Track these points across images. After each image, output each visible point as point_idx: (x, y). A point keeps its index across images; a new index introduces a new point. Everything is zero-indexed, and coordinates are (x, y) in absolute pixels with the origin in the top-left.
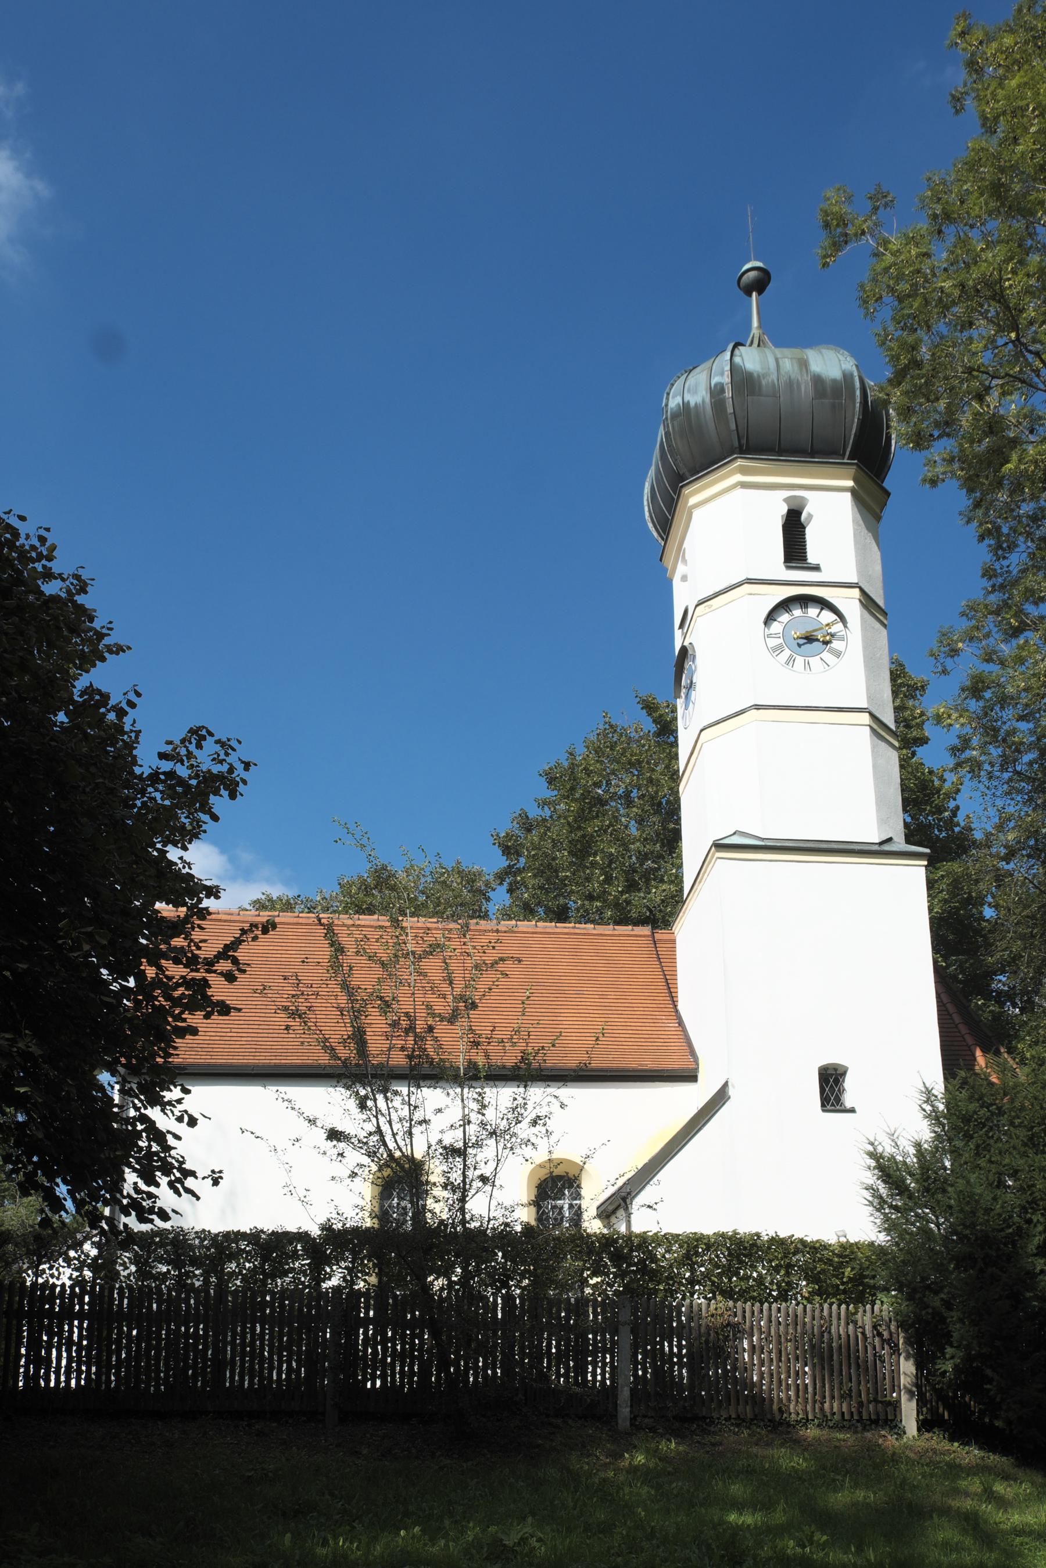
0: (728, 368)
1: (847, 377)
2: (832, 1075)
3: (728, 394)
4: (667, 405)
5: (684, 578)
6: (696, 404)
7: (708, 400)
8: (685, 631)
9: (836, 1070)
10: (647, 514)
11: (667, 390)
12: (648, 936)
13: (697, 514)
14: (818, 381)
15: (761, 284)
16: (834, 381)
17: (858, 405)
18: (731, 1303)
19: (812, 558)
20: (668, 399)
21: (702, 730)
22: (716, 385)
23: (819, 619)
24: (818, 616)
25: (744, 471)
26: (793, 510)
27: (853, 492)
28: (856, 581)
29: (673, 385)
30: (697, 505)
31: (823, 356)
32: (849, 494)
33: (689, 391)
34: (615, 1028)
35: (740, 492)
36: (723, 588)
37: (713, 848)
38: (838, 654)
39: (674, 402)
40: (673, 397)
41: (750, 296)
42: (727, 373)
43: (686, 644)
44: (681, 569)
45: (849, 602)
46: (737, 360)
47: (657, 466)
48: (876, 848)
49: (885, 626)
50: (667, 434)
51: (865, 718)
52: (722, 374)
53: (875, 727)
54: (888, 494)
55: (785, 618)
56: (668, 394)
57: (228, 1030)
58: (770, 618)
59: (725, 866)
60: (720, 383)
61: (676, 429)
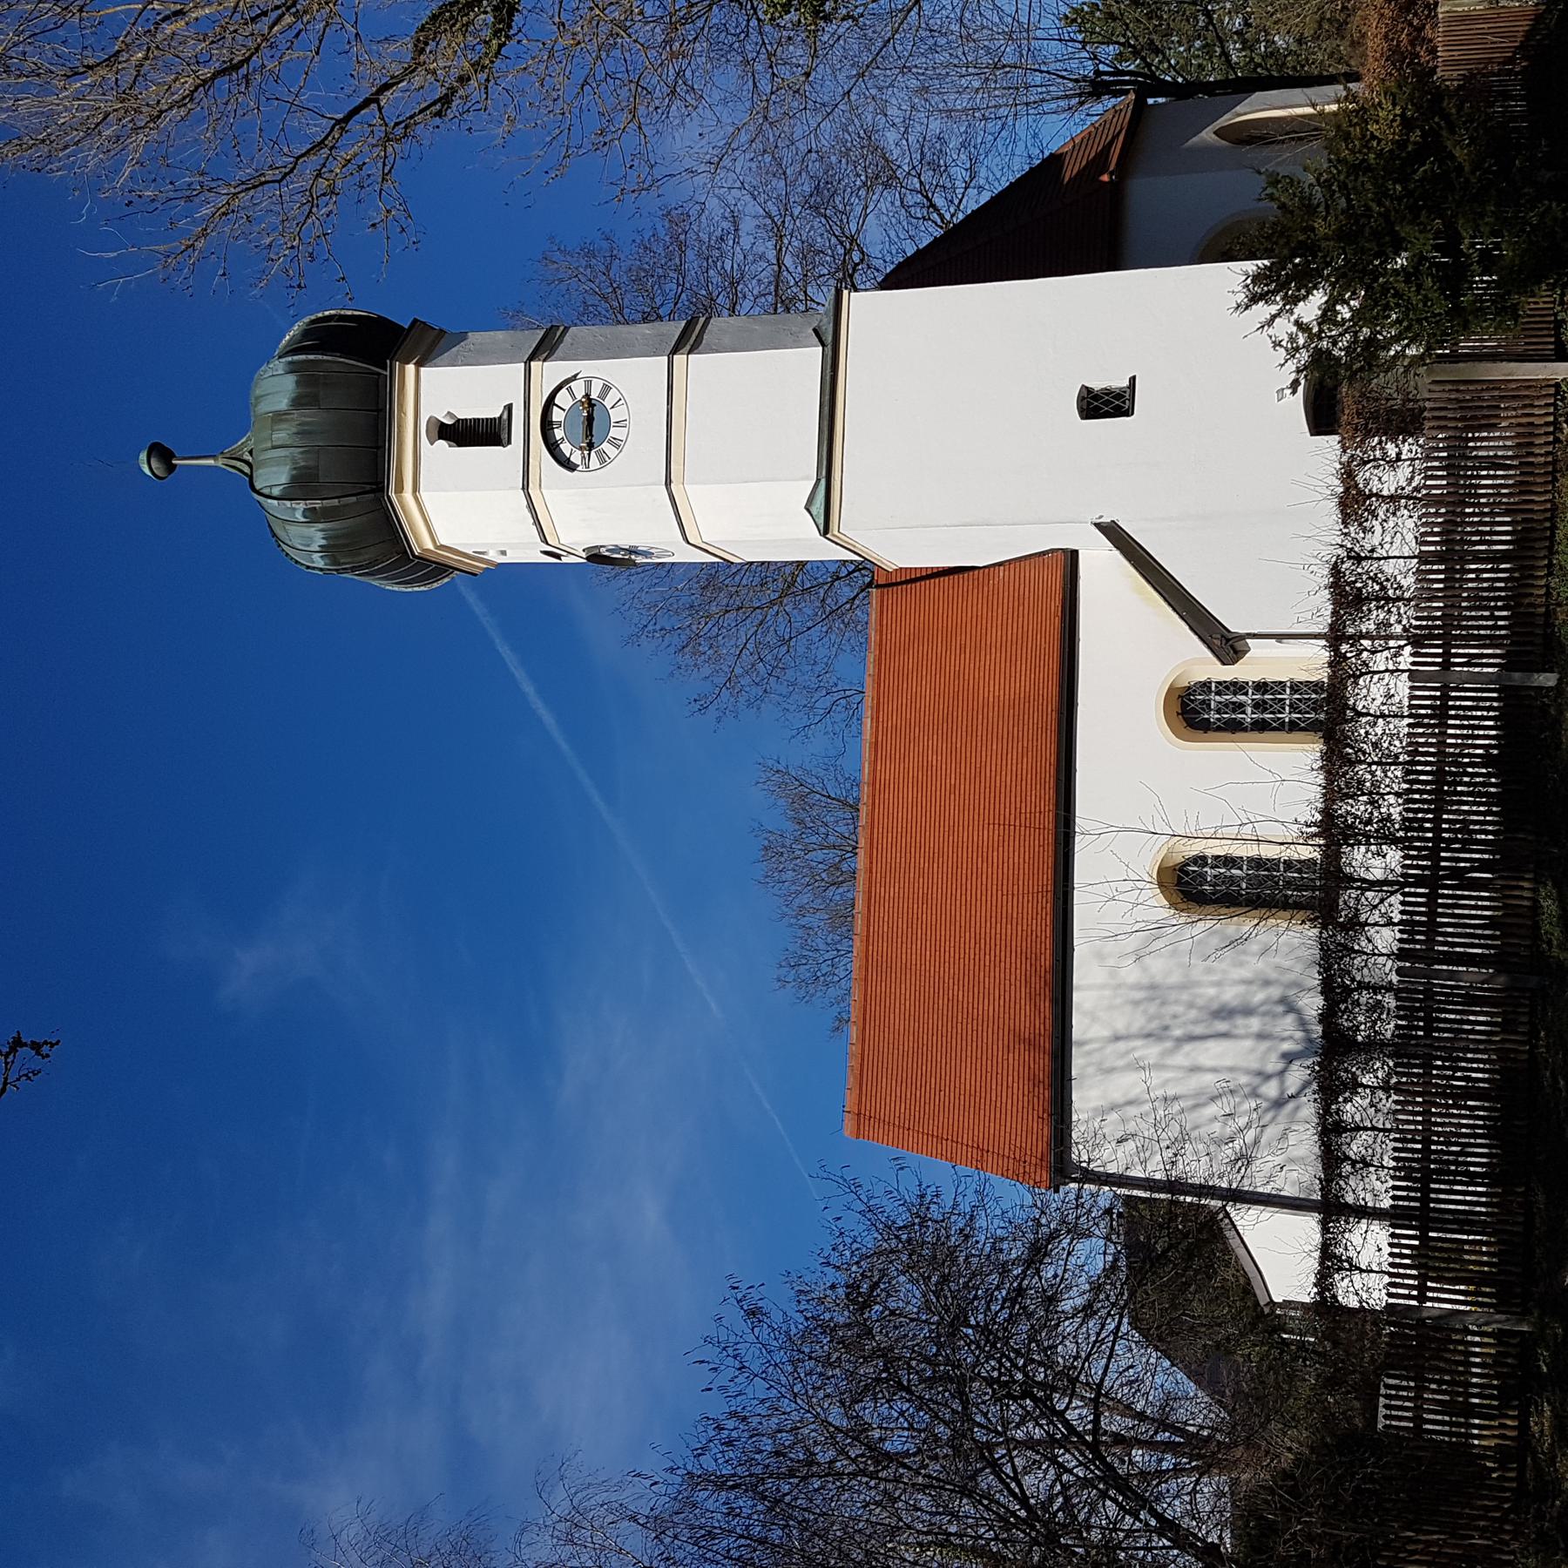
0: (288, 503)
1: (293, 368)
2: (1089, 404)
3: (318, 504)
4: (321, 570)
5: (504, 553)
6: (323, 538)
7: (321, 526)
8: (565, 554)
9: (1084, 398)
10: (422, 588)
11: (303, 568)
12: (882, 594)
13: (443, 541)
14: (297, 403)
15: (162, 453)
16: (298, 383)
17: (325, 357)
18: (1377, 1206)
19: (495, 413)
20: (314, 568)
21: (688, 543)
22: (305, 517)
23: (567, 408)
24: (564, 410)
25: (400, 489)
26: (439, 432)
27: (419, 365)
28: (523, 364)
29: (297, 562)
30: (434, 541)
31: (262, 396)
32: (422, 369)
33: (308, 546)
34: (1004, 638)
35: (424, 495)
36: (530, 515)
37: (828, 536)
38: (606, 389)
39: (318, 561)
40: (313, 562)
41: (176, 465)
42: (294, 504)
43: (584, 555)
44: (494, 556)
45: (549, 373)
46: (276, 492)
47: (374, 580)
48: (829, 349)
49: (566, 329)
50: (353, 569)
51: (679, 359)
52: (294, 509)
53: (688, 347)
54: (415, 321)
55: (566, 448)
56: (308, 567)
57: (1005, 1062)
58: (568, 465)
59: (849, 521)
60: (304, 512)
61: (349, 560)
